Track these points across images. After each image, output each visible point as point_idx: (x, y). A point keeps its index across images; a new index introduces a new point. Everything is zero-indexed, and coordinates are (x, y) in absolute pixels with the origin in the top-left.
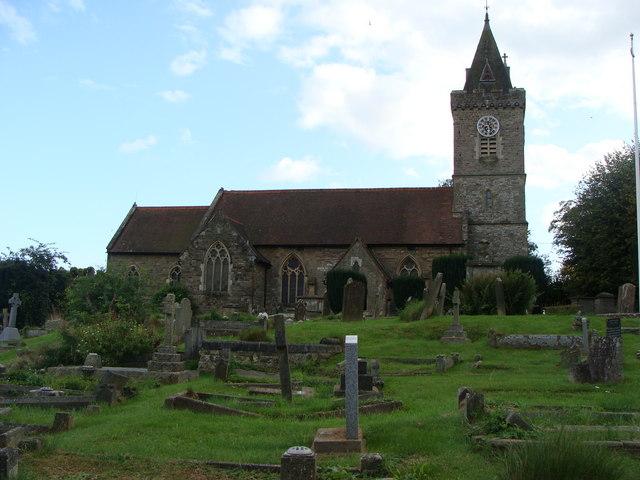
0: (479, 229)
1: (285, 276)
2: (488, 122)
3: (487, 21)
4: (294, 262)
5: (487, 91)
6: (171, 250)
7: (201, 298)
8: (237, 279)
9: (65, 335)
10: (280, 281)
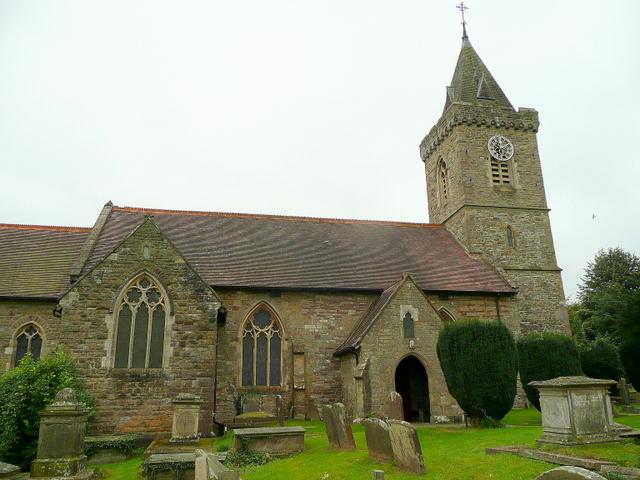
1: (248, 339)
3: (465, 37)
4: (263, 316)
6: (39, 293)
7: (106, 383)
8: (183, 345)
9: (144, 465)
10: (240, 349)
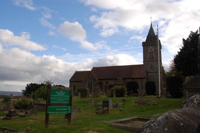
0: (149, 74)
1: (105, 86)
2: (151, 49)
3: (151, 25)
4: (107, 83)
5: (151, 41)
